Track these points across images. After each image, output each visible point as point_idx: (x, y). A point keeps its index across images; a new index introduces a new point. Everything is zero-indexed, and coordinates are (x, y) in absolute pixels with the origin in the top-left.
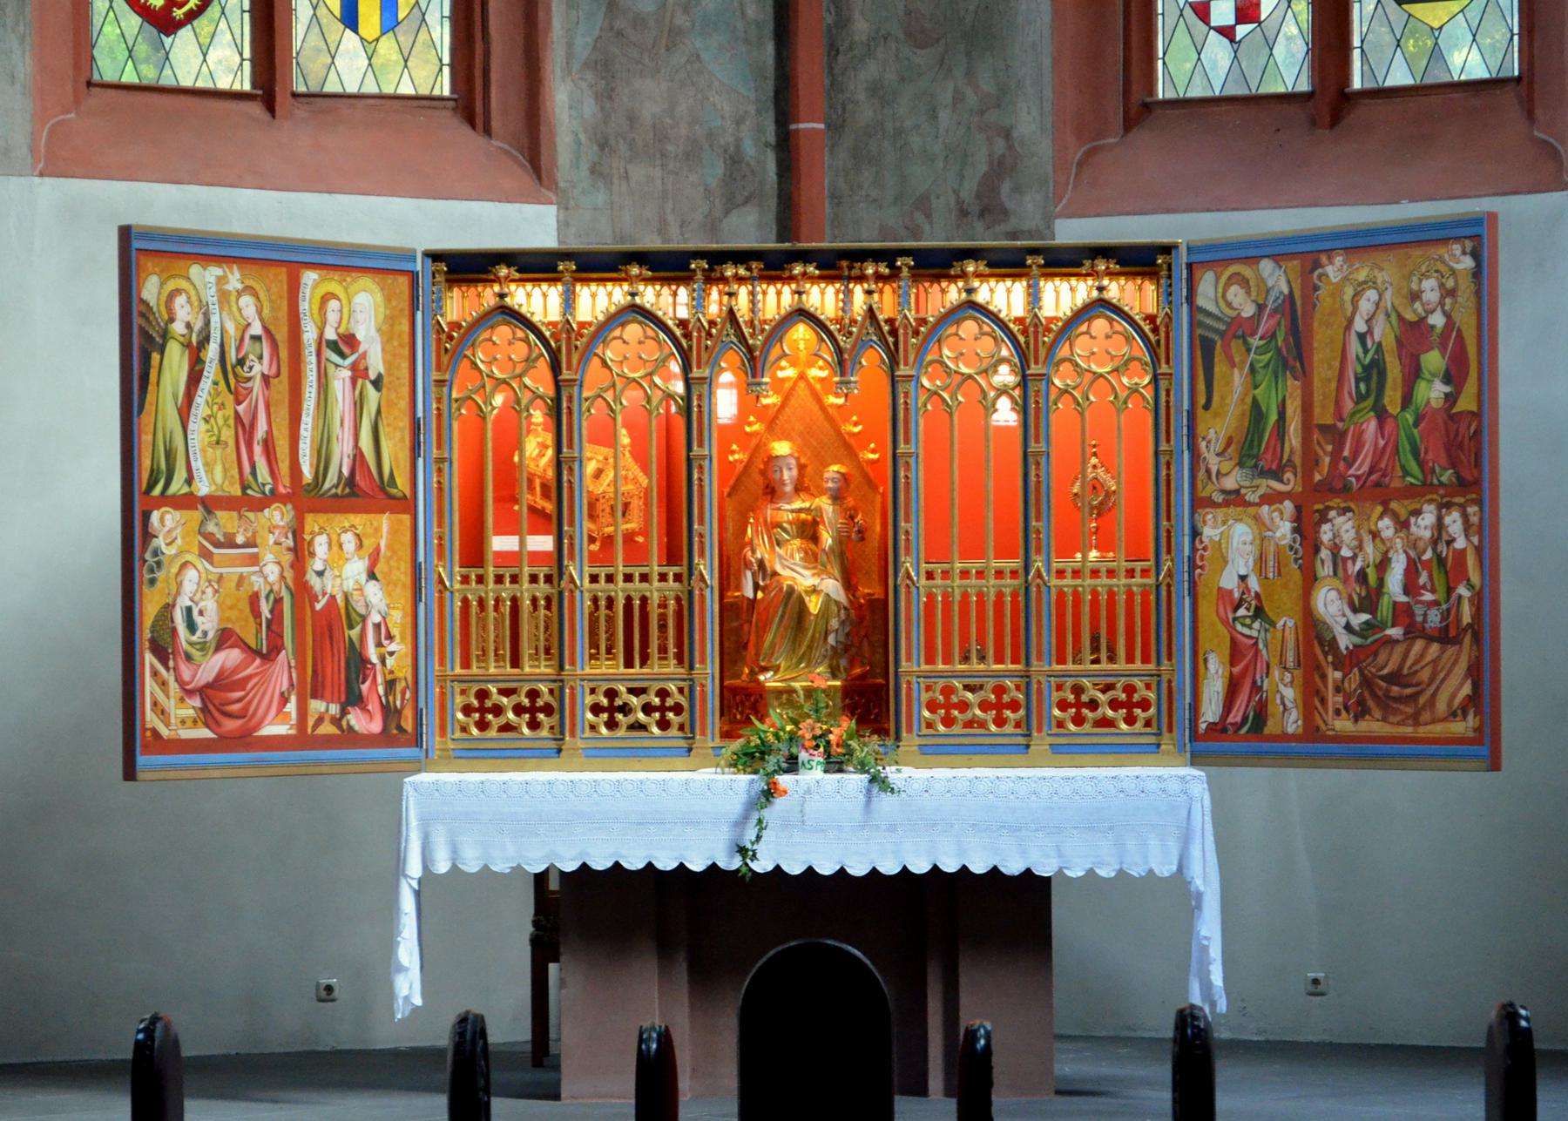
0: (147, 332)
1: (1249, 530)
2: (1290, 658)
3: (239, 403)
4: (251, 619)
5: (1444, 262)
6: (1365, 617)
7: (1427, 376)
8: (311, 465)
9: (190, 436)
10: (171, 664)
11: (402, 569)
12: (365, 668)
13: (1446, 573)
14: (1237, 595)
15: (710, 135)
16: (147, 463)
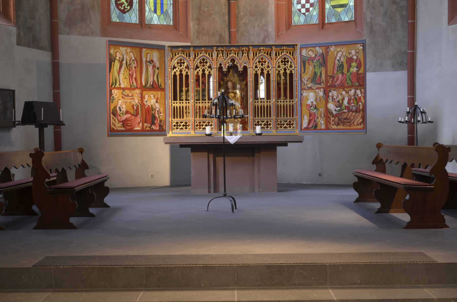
0: (111, 59)
1: (313, 94)
2: (323, 116)
3: (130, 71)
4: (133, 109)
5: (356, 48)
6: (339, 108)
7: (353, 67)
8: (144, 82)
9: (120, 77)
10: (116, 117)
11: (163, 101)
12: (155, 118)
13: (357, 100)
14: (311, 105)
15: (217, 32)
16: (111, 81)
